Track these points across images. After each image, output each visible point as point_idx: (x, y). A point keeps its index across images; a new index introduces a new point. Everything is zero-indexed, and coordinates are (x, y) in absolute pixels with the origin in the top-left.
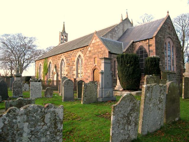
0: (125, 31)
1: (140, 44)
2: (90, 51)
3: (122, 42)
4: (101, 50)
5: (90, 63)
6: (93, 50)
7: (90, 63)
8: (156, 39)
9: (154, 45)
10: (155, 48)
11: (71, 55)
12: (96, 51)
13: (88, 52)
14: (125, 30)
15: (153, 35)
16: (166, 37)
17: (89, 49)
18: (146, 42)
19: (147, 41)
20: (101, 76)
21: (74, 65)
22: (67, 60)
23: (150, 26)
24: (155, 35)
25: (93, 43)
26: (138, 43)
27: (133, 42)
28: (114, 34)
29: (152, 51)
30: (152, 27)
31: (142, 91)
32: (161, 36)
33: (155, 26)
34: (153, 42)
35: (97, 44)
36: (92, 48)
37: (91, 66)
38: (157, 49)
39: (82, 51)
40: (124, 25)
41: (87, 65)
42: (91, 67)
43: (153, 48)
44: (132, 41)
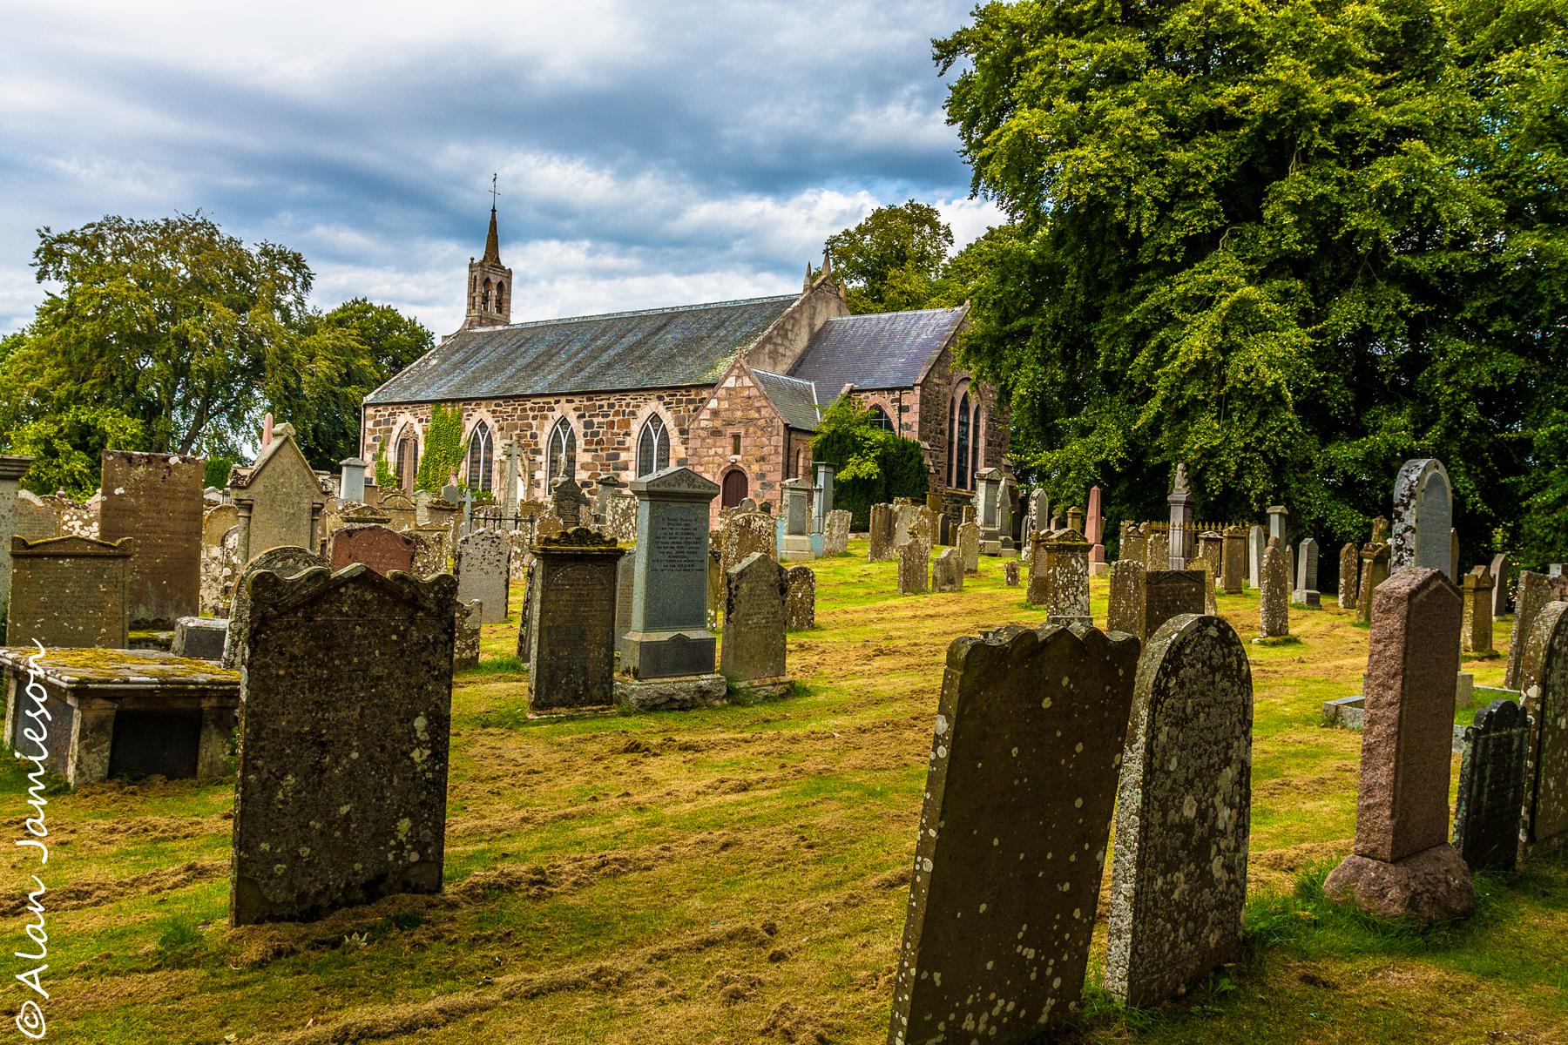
0: (816, 329)
1: (875, 399)
2: (715, 413)
3: (809, 379)
4: (757, 415)
5: (712, 452)
6: (726, 410)
7: (712, 452)
8: (922, 390)
9: (916, 408)
10: (917, 418)
11: (611, 406)
12: (739, 414)
13: (705, 415)
14: (819, 323)
15: (916, 375)
16: (956, 380)
17: (713, 404)
18: (892, 397)
19: (897, 393)
20: (647, 512)
21: (624, 449)
22: (588, 425)
23: (908, 334)
24: (919, 381)
25: (727, 389)
26: (869, 394)
27: (852, 391)
28: (782, 345)
29: (908, 427)
30: (916, 338)
31: (798, 338)
32: (939, 378)
33: (924, 336)
34: (913, 399)
35: (746, 393)
36: (725, 405)
37: (718, 460)
38: (923, 420)
39: (667, 399)
40: (815, 308)
41: (700, 457)
42: (719, 465)
43: (913, 417)
44: (848, 386)
